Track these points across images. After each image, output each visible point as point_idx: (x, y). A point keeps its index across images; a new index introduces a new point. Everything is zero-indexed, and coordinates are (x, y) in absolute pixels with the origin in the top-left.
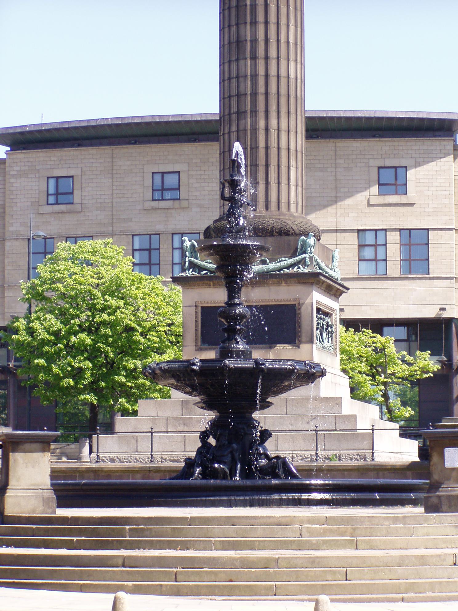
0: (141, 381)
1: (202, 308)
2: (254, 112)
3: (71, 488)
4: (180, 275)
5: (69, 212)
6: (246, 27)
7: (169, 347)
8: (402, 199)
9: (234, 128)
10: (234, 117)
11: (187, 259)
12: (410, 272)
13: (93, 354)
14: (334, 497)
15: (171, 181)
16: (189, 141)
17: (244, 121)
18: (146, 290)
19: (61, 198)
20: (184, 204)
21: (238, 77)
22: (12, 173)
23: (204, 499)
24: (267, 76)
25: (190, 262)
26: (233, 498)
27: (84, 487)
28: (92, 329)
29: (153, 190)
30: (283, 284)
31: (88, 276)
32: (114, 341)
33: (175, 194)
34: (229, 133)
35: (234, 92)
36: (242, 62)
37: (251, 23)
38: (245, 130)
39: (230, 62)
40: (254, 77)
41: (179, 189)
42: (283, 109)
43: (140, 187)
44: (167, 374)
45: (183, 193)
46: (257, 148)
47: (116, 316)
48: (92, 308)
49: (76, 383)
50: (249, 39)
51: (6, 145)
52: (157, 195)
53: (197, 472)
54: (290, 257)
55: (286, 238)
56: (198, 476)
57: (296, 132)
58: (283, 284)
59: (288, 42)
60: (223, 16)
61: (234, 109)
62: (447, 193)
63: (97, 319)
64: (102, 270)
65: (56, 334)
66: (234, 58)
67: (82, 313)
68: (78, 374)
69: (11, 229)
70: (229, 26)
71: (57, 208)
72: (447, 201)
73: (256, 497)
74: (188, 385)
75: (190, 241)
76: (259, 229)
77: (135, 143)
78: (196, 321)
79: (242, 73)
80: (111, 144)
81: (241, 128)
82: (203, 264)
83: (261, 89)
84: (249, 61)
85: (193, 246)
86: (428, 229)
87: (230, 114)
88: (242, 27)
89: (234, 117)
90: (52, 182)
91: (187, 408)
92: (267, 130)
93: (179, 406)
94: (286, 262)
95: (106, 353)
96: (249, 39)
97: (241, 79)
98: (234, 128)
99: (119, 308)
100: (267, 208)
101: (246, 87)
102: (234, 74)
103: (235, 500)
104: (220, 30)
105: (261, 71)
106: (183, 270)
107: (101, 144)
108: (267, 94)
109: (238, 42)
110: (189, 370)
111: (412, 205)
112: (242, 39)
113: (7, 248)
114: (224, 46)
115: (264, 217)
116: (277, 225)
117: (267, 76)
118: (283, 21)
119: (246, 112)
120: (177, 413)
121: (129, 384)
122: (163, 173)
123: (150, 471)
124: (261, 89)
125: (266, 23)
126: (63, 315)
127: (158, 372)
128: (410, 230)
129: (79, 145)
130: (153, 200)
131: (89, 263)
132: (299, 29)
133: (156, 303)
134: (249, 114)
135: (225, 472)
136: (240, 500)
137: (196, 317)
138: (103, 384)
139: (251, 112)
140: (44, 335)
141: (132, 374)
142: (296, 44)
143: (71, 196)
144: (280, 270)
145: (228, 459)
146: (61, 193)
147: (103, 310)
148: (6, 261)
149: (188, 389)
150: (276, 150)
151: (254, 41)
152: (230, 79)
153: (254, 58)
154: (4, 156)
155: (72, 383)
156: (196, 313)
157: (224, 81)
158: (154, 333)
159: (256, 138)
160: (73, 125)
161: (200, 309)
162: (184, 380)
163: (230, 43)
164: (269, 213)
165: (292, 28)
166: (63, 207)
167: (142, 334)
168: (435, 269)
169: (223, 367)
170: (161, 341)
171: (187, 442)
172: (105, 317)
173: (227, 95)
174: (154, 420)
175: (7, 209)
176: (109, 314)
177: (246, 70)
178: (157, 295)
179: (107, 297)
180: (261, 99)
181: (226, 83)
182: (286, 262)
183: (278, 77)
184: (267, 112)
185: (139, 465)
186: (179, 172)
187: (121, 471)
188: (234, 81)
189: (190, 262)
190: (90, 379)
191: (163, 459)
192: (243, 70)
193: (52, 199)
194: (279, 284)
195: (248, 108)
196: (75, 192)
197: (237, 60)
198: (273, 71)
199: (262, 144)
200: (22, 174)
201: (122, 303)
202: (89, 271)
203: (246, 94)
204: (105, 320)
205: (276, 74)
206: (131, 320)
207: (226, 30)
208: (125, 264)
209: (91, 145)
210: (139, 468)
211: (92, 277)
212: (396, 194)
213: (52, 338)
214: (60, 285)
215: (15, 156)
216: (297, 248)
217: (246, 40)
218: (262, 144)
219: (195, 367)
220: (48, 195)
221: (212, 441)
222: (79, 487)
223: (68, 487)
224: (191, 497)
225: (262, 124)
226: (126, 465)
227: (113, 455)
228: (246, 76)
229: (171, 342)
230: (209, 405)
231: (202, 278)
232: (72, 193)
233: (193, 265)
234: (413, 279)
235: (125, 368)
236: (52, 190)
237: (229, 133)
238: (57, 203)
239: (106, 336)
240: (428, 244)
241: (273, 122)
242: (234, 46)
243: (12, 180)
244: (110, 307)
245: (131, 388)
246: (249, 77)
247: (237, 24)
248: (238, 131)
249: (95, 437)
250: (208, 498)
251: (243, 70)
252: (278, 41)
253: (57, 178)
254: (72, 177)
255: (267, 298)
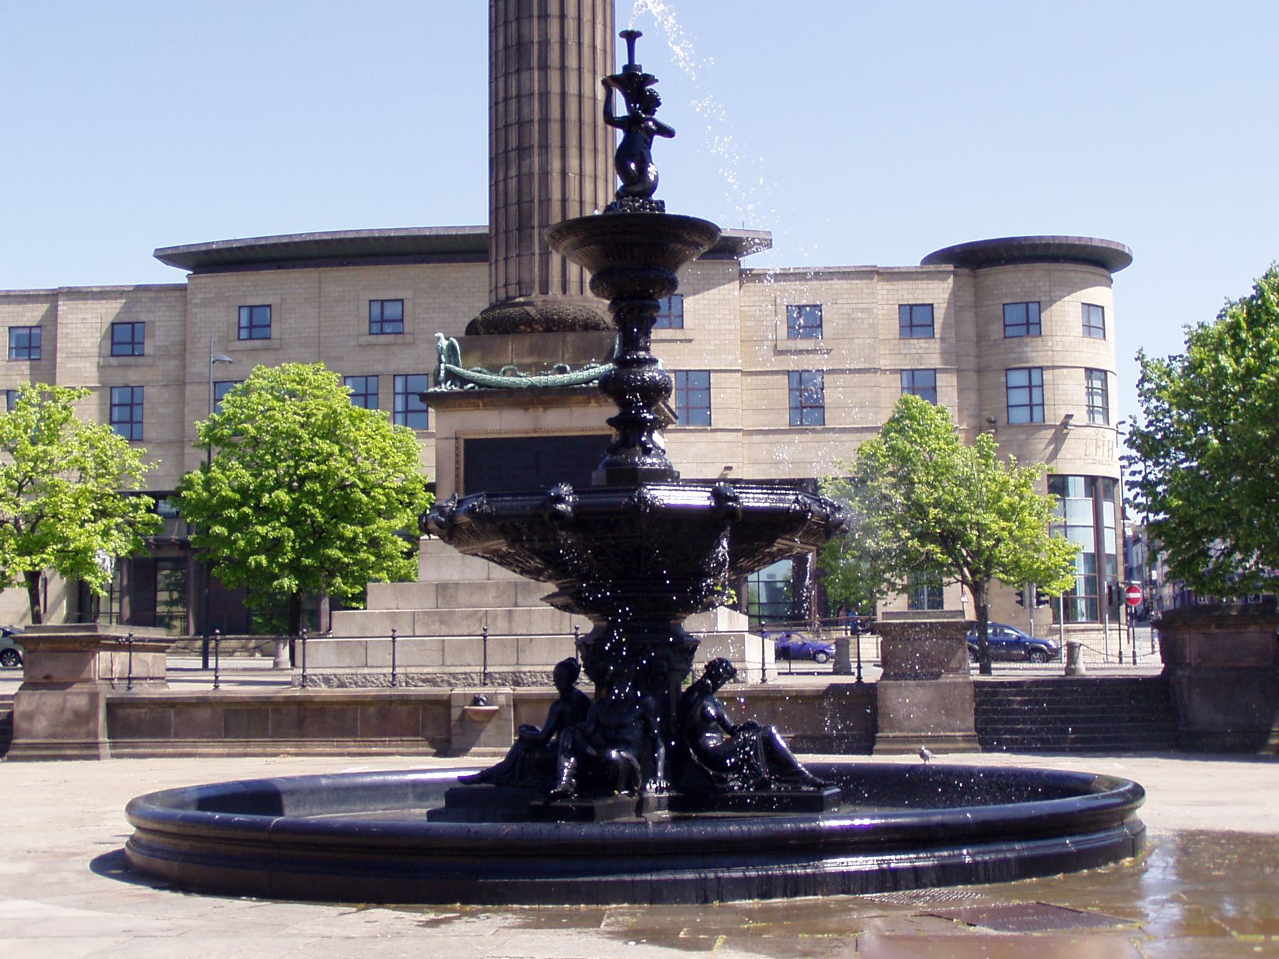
0: (362, 555)
1: (466, 441)
2: (545, 147)
3: (240, 834)
4: (432, 390)
5: (265, 349)
6: (531, 22)
7: (399, 510)
8: (677, 334)
9: (513, 172)
10: (513, 155)
11: (442, 366)
12: (688, 423)
13: (296, 518)
14: (978, 858)
15: (392, 311)
16: (416, 262)
17: (528, 161)
18: (369, 431)
19: (256, 332)
20: (409, 339)
21: (519, 96)
22: (195, 301)
23: (627, 878)
24: (563, 95)
25: (448, 371)
26: (712, 875)
27: (276, 837)
28: (296, 484)
29: (371, 322)
30: (593, 404)
31: (287, 416)
32: (326, 501)
33: (398, 327)
34: (505, 179)
35: (513, 118)
36: (525, 75)
37: (539, 17)
38: (531, 175)
39: (506, 75)
40: (545, 95)
41: (402, 320)
42: (588, 145)
43: (355, 319)
44: (488, 526)
45: (408, 326)
46: (549, 200)
47: (329, 466)
48: (296, 455)
49: (270, 562)
50: (536, 39)
51: (188, 268)
52: (376, 328)
53: (566, 771)
54: (602, 364)
55: (595, 334)
56: (569, 782)
57: (606, 180)
58: (593, 404)
59: (594, 47)
60: (496, 12)
61: (514, 143)
62: (732, 327)
63: (301, 471)
64: (312, 404)
65: (243, 490)
66: (513, 69)
67: (281, 461)
68: (272, 547)
69: (193, 370)
70: (506, 23)
71: (250, 344)
72: (732, 337)
73: (776, 871)
74: (536, 553)
75: (447, 339)
76: (554, 321)
77: (349, 264)
78: (457, 462)
79: (525, 91)
80: (318, 265)
81: (525, 170)
82: (469, 373)
83: (555, 113)
84: (536, 73)
85: (451, 346)
86: (709, 371)
87: (506, 152)
88: (525, 23)
89: (513, 155)
90: (245, 313)
91: (444, 597)
92: (564, 173)
93: (433, 595)
94: (597, 370)
95: (312, 516)
96: (536, 39)
97: (524, 100)
98: (513, 172)
99: (331, 455)
100: (564, 290)
101: (532, 111)
102: (513, 92)
103: (718, 879)
104: (490, 32)
105: (555, 87)
106: (437, 383)
107: (306, 266)
108: (563, 120)
109: (519, 44)
110: (546, 517)
111: (690, 341)
112: (526, 40)
113: (187, 394)
114: (496, 52)
115: (560, 303)
116: (582, 316)
117: (563, 95)
118: (587, 16)
119: (531, 147)
120: (428, 604)
121: (346, 560)
122: (383, 302)
123: (391, 702)
124: (555, 113)
125: (563, 16)
126: (256, 467)
127: (463, 519)
128: (687, 371)
129: (279, 268)
130: (370, 334)
131: (292, 394)
132: (609, 31)
133: (382, 449)
134: (536, 150)
135: (632, 767)
136: (732, 879)
137: (457, 455)
138: (308, 562)
139: (540, 147)
140: (227, 492)
141: (350, 546)
142: (605, 51)
143: (267, 330)
144: (587, 382)
145: (635, 734)
146: (256, 326)
147: (310, 459)
148: (187, 409)
149: (536, 563)
150: (577, 204)
151: (544, 44)
152: (506, 100)
153: (544, 67)
154: (186, 281)
155: (263, 560)
156: (457, 448)
157: (496, 103)
158: (380, 491)
159: (547, 186)
160: (271, 241)
161: (462, 443)
162: (530, 540)
163: (506, 48)
164: (566, 298)
165: (599, 27)
166: (258, 343)
167: (363, 491)
168: (718, 420)
169: (636, 507)
170: (389, 503)
171: (447, 650)
172: (313, 466)
173: (501, 124)
174: (393, 616)
175: (188, 345)
176: (318, 463)
177: (532, 86)
178: (383, 437)
179: (316, 439)
180: (555, 129)
181: (501, 107)
182: (597, 370)
183: (580, 96)
184: (563, 147)
185: (371, 691)
186: (402, 300)
187: (343, 703)
188: (513, 103)
189: (448, 371)
190: (290, 555)
191: (409, 680)
192: (527, 86)
193: (244, 334)
194: (587, 402)
195: (536, 142)
196: (273, 324)
197: (518, 71)
198: (572, 88)
199: (556, 195)
200: (207, 303)
201: (336, 449)
202: (291, 405)
203: (532, 121)
204: (312, 471)
205: (576, 92)
206: (348, 472)
207: (501, 30)
208: (341, 398)
209: (294, 267)
210: (374, 696)
211: (295, 413)
212: (670, 327)
213: (238, 496)
214: (247, 426)
215: (199, 281)
216: (613, 349)
217: (532, 42)
218: (556, 195)
219: (561, 507)
220: (240, 328)
221: (585, 685)
222: (263, 836)
223: (229, 833)
224: (593, 875)
225: (556, 165)
226: (353, 690)
227: (327, 671)
228: (532, 94)
229: (401, 503)
230: (571, 601)
231: (468, 394)
232: (269, 326)
233: (451, 375)
234: (691, 431)
235: (341, 537)
236: (244, 322)
237: (505, 179)
238: (250, 338)
239: (313, 494)
240: (709, 389)
241: (573, 163)
242: (513, 50)
243: (194, 310)
244: (318, 454)
245: (348, 565)
246: (536, 97)
247: (518, 20)
248: (519, 176)
249: (299, 642)
250: (638, 878)
251: (527, 86)
252: (580, 44)
253: (251, 307)
254: (270, 306)
255: (567, 425)
